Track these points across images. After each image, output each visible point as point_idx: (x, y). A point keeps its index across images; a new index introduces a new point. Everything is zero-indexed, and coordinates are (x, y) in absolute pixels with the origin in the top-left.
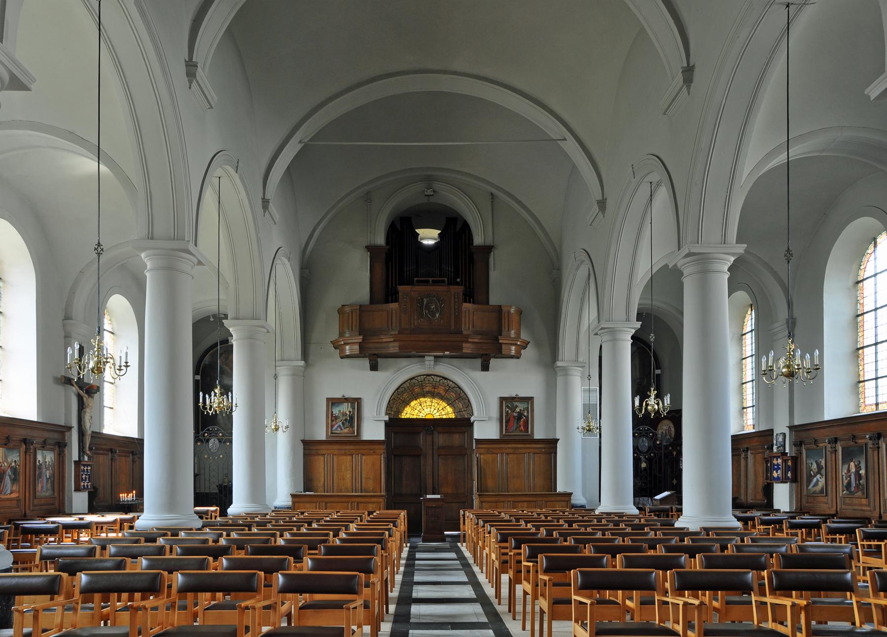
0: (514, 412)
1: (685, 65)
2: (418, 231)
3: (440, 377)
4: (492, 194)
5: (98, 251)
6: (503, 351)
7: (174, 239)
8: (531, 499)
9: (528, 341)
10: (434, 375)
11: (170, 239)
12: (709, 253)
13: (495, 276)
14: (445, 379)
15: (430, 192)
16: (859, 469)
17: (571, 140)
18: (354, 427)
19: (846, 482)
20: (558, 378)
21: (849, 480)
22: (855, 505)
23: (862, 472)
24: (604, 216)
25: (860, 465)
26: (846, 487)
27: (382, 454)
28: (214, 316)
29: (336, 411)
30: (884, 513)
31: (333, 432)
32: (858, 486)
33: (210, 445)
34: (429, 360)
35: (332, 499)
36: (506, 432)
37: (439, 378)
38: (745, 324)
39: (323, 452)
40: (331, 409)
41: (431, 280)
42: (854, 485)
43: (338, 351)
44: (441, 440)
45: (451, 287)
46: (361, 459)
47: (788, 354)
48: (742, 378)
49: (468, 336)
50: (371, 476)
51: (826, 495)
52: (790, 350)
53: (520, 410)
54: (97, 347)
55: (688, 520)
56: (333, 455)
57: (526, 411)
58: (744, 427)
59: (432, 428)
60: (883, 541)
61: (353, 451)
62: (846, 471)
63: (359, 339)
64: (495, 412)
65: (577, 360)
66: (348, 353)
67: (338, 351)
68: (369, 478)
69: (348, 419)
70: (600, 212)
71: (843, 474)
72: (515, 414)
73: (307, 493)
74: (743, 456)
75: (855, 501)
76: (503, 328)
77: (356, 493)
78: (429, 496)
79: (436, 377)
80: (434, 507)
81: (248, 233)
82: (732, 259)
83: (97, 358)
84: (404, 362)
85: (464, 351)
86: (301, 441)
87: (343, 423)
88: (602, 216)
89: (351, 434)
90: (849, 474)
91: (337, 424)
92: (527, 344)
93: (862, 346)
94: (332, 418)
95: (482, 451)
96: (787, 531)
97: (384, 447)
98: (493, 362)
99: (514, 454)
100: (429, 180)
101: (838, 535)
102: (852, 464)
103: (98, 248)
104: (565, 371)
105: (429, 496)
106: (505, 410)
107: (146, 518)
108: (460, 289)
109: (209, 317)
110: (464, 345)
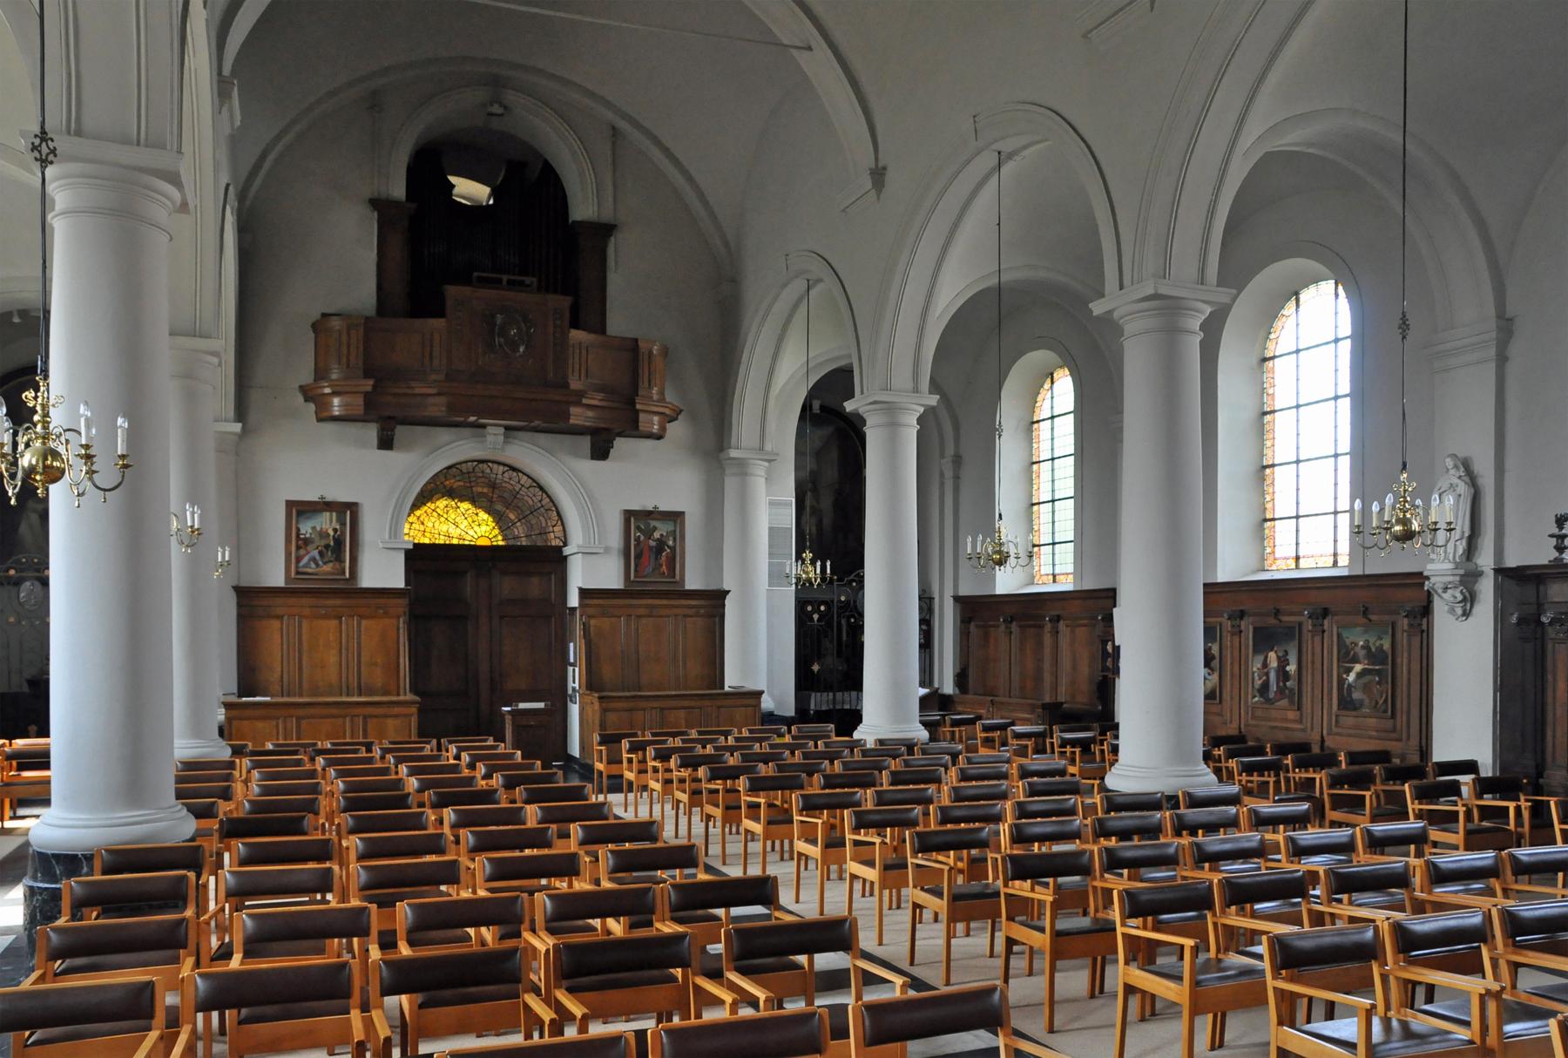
0: (650, 538)
1: (874, 166)
2: (453, 179)
3: (504, 465)
4: (614, 128)
5: (40, 152)
6: (640, 424)
7: (138, 143)
8: (693, 703)
9: (682, 408)
10: (493, 462)
11: (125, 141)
12: (1184, 298)
13: (617, 283)
14: (514, 469)
15: (496, 109)
16: (1284, 663)
17: (822, 51)
18: (344, 562)
19: (1258, 683)
20: (726, 478)
21: (1264, 681)
22: (1275, 720)
23: (1292, 668)
24: (878, 198)
25: (1288, 657)
26: (1259, 691)
27: (398, 617)
28: (23, 313)
29: (306, 528)
30: (1328, 734)
31: (301, 570)
32: (1281, 691)
33: (22, 595)
34: (494, 433)
35: (312, 711)
36: (635, 577)
37: (501, 468)
38: (1037, 405)
39: (279, 611)
40: (297, 522)
41: (505, 278)
42: (1275, 689)
43: (312, 407)
44: (506, 586)
45: (550, 297)
46: (359, 625)
47: (1402, 499)
48: (1031, 496)
49: (580, 394)
50: (379, 661)
51: (1221, 702)
52: (1405, 493)
53: (662, 535)
54: (40, 412)
55: (1142, 775)
56: (301, 617)
57: (671, 538)
58: (1034, 577)
59: (490, 565)
60: (1369, 789)
61: (340, 609)
62: (1259, 666)
63: (368, 385)
64: (614, 536)
65: (762, 449)
66: (336, 412)
67: (312, 407)
68: (376, 664)
69: (332, 543)
70: (874, 190)
71: (1255, 669)
72: (652, 543)
73: (244, 699)
74: (1048, 627)
75: (1274, 714)
76: (640, 384)
77: (348, 695)
78: (522, 706)
79: (495, 466)
80: (531, 726)
81: (197, 145)
82: (1208, 310)
83: (40, 441)
84: (444, 435)
85: (571, 421)
86: (232, 591)
87: (321, 553)
88: (875, 197)
89: (338, 574)
90: (1266, 670)
91: (308, 553)
92: (678, 415)
93: (1270, 463)
94: (297, 543)
95: (590, 611)
96: (1240, 778)
97: (404, 602)
98: (620, 444)
99: (649, 616)
100: (496, 83)
101: (1255, 774)
102: (1272, 655)
103: (40, 145)
104: (742, 467)
105: (522, 706)
106: (635, 534)
107: (49, 822)
108: (565, 302)
109: (10, 314)
110: (574, 410)
